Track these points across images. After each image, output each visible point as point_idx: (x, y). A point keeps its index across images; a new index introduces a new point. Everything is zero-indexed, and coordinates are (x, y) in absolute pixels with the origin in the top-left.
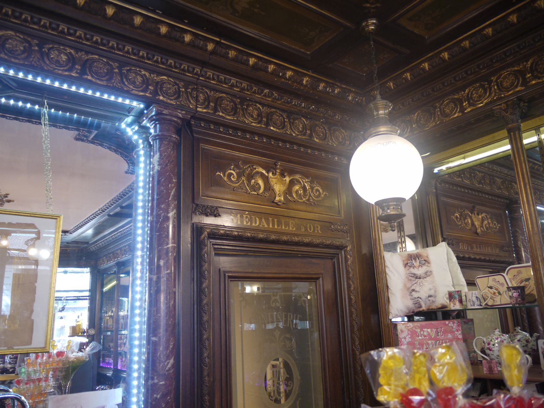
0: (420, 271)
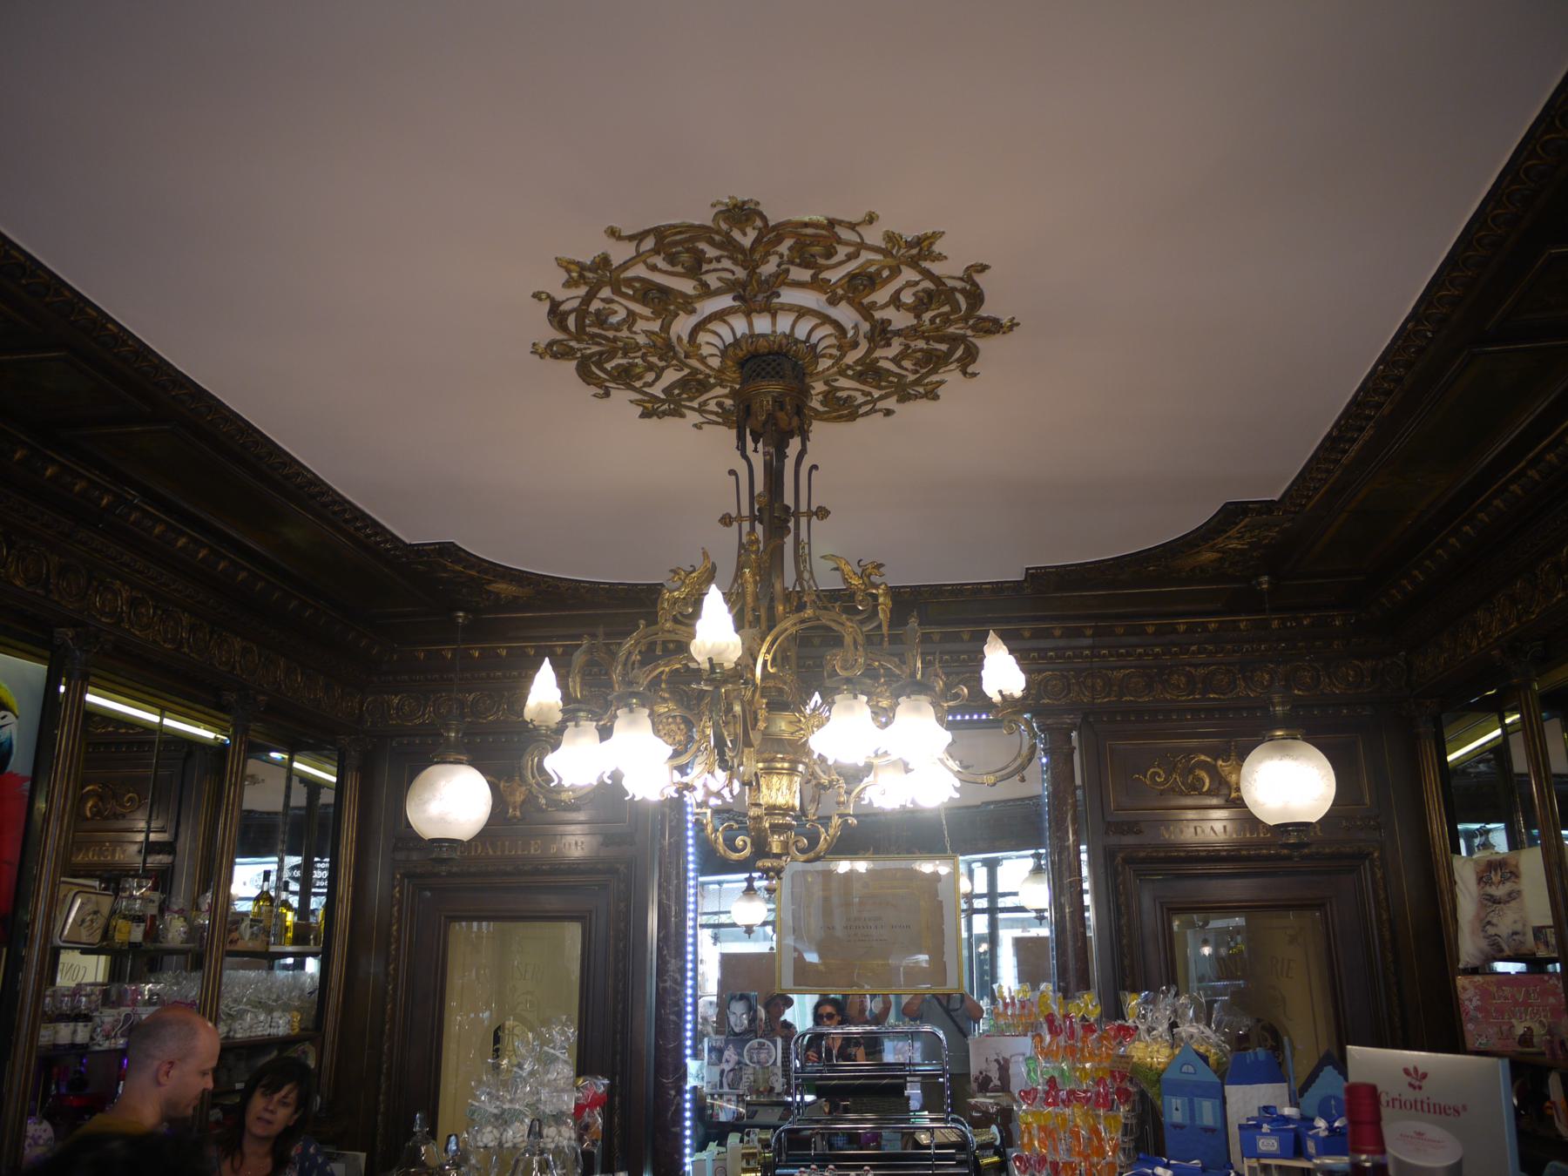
0: (1499, 891)
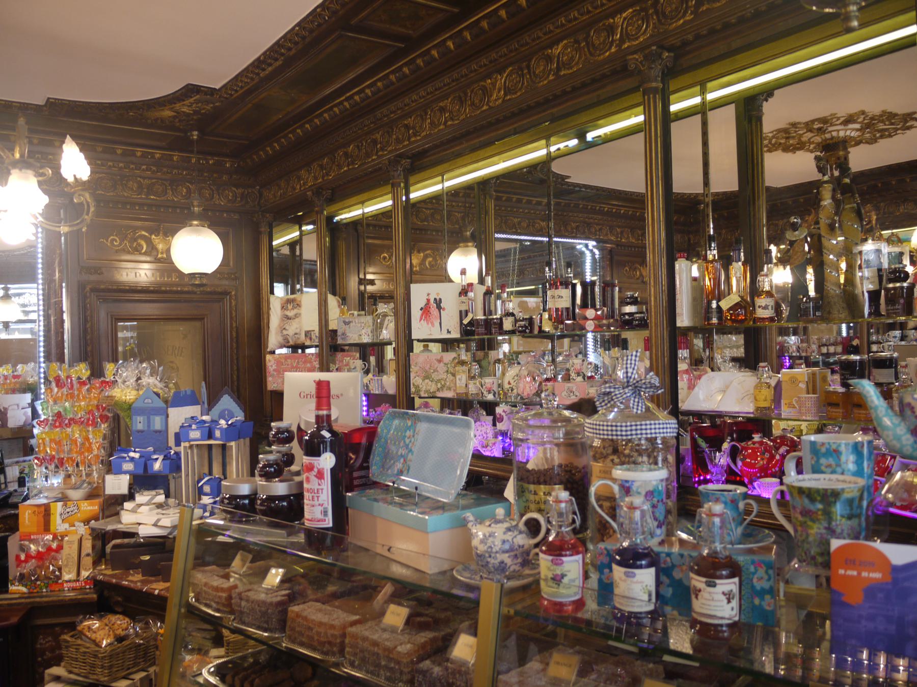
0: (291, 314)
